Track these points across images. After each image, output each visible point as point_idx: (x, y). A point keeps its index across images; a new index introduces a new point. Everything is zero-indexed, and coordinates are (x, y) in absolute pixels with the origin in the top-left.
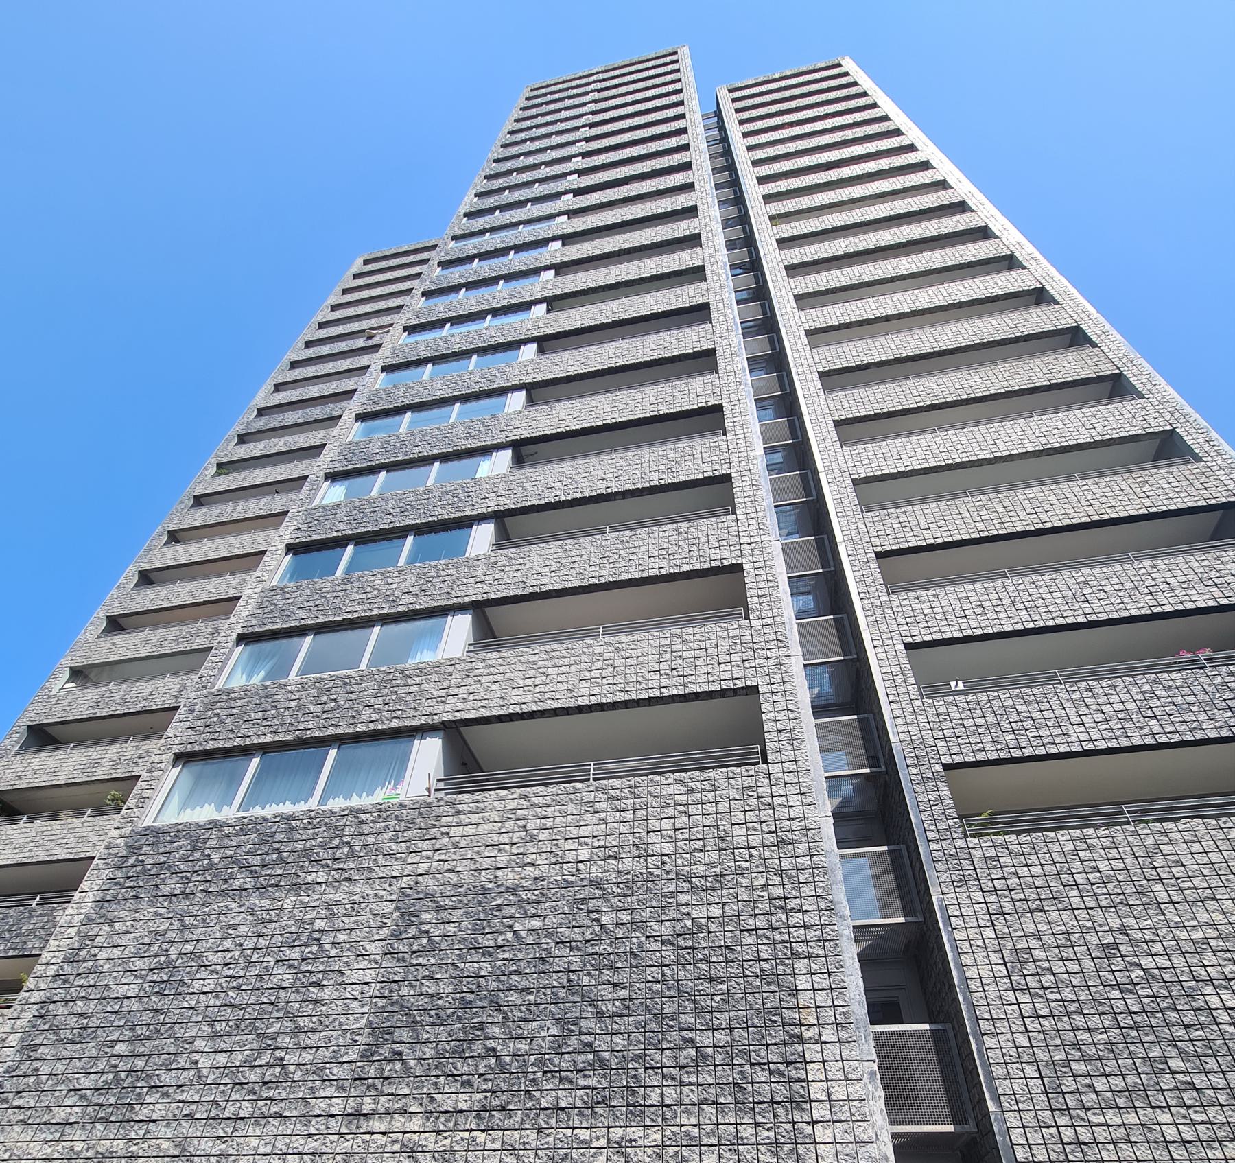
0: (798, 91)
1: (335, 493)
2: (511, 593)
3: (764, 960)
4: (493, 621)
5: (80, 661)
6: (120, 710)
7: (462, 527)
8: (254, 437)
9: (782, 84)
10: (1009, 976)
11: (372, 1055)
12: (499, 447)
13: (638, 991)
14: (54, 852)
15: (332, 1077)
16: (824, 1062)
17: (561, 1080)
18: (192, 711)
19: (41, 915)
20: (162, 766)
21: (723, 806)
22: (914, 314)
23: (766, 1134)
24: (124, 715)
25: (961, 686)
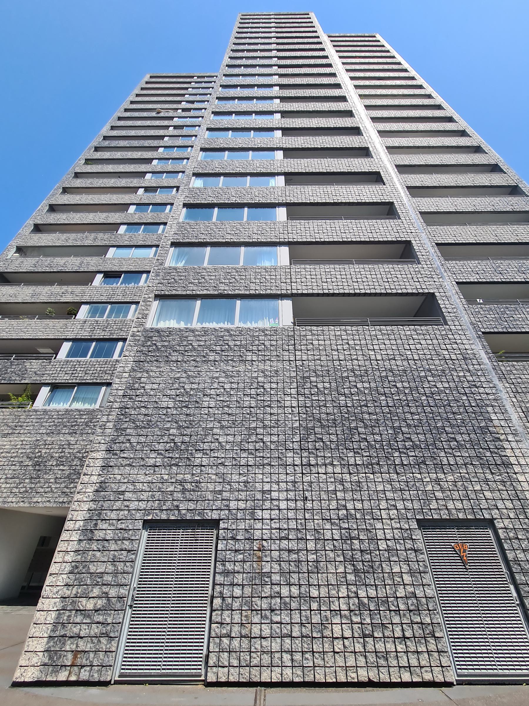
0: (359, 44)
1: (198, 183)
2: (217, 240)
3: (308, 407)
4: (302, 251)
5: (22, 244)
6: (48, 270)
7: (210, 208)
8: (104, 149)
9: (352, 39)
10: (526, 417)
11: (115, 440)
12: (278, 174)
13: (239, 418)
14: (20, 335)
15: (155, 449)
16: (512, 449)
17: (158, 454)
18: (157, 275)
19: (18, 364)
20: (151, 300)
21: (280, 342)
22: (429, 147)
23: (498, 477)
24: (50, 272)
25: (481, 301)
